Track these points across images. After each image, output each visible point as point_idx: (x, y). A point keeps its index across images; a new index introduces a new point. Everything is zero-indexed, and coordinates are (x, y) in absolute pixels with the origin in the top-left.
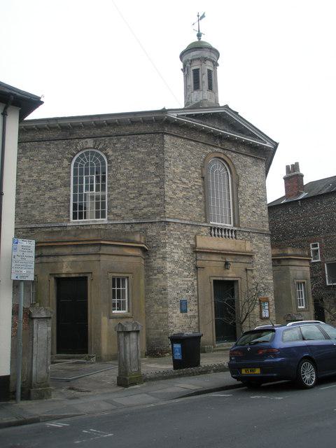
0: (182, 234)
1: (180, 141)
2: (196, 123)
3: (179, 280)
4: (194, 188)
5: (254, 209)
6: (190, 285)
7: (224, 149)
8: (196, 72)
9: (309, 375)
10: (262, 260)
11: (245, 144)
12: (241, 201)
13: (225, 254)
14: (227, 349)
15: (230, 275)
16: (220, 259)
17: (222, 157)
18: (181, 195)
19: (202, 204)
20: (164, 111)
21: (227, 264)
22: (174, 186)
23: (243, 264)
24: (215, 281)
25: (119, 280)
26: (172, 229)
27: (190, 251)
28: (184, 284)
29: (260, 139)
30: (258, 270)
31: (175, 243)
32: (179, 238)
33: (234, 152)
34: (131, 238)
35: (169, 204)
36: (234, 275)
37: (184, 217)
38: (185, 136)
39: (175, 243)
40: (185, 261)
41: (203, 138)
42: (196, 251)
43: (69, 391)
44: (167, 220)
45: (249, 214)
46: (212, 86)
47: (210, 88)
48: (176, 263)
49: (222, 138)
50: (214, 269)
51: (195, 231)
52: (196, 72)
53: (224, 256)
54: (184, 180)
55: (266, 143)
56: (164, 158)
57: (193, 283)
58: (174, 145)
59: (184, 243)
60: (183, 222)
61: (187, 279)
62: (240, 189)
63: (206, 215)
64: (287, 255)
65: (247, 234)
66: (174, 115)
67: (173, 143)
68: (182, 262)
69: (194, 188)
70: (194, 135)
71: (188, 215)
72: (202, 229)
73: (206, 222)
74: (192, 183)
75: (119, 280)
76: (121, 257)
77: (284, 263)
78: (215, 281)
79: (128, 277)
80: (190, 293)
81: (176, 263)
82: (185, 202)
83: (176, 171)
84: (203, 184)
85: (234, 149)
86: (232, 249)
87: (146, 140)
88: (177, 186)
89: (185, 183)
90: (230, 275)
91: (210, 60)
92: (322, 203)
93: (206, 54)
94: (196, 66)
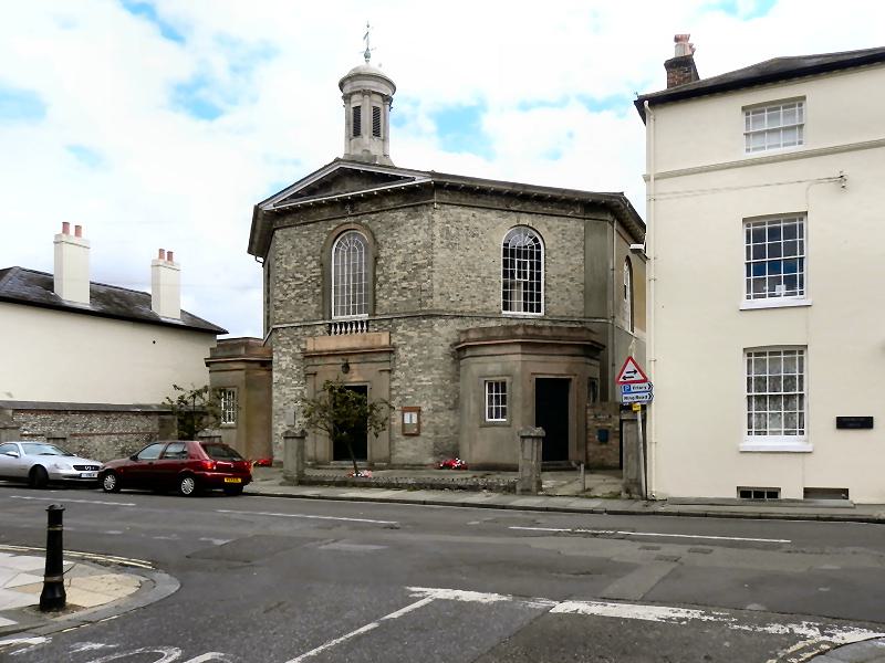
1: (293, 231)
2: (298, 203)
3: (286, 390)
5: (405, 284)
8: (357, 110)
9: (188, 485)
10: (411, 355)
11: (397, 191)
12: (381, 279)
13: (346, 354)
15: (355, 378)
16: (341, 361)
18: (293, 295)
19: (320, 297)
23: (374, 365)
24: (538, 381)
25: (497, 384)
27: (300, 356)
30: (405, 370)
31: (284, 350)
34: (236, 352)
37: (297, 319)
39: (284, 350)
41: (326, 212)
42: (308, 356)
43: (642, 551)
45: (396, 292)
50: (330, 372)
52: (357, 110)
53: (345, 357)
54: (298, 275)
59: (294, 349)
62: (381, 262)
63: (325, 311)
65: (386, 323)
71: (301, 316)
72: (318, 329)
74: (309, 275)
78: (538, 381)
81: (283, 371)
83: (288, 268)
85: (373, 209)
90: (353, 380)
94: (356, 100)
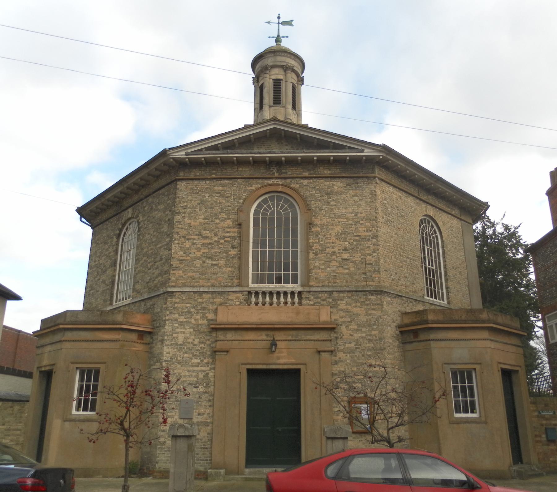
0: (193, 307)
1: (202, 185)
4: (222, 241)
6: (201, 376)
7: (285, 178)
10: (357, 335)
11: (338, 161)
12: (316, 247)
14: (259, 479)
17: (280, 189)
18: (198, 254)
20: (164, 153)
21: (274, 344)
22: (188, 244)
26: (177, 300)
28: (190, 376)
29: (350, 148)
31: (182, 319)
32: (189, 312)
33: (306, 178)
34: (110, 318)
35: (176, 268)
36: (293, 361)
37: (201, 283)
38: (214, 176)
39: (182, 319)
40: (196, 342)
41: (246, 171)
44: (170, 290)
45: (335, 263)
46: (295, 105)
47: (294, 107)
48: (180, 347)
49: (277, 163)
51: (218, 300)
54: (207, 233)
55: (363, 151)
56: (174, 211)
57: (207, 374)
58: (192, 192)
59: (197, 319)
60: (196, 289)
61: (199, 368)
64: (427, 322)
66: (181, 155)
67: (191, 189)
68: (190, 345)
69: (222, 241)
70: (229, 172)
73: (239, 285)
75: (90, 372)
76: (91, 343)
77: (422, 337)
79: (475, 369)
80: (201, 389)
81: (180, 347)
82: (204, 262)
84: (240, 233)
85: (306, 174)
86: (289, 320)
87: (164, 194)
88: (193, 244)
89: (207, 237)
91: (294, 71)
92: (179, 213)
93: (292, 62)
